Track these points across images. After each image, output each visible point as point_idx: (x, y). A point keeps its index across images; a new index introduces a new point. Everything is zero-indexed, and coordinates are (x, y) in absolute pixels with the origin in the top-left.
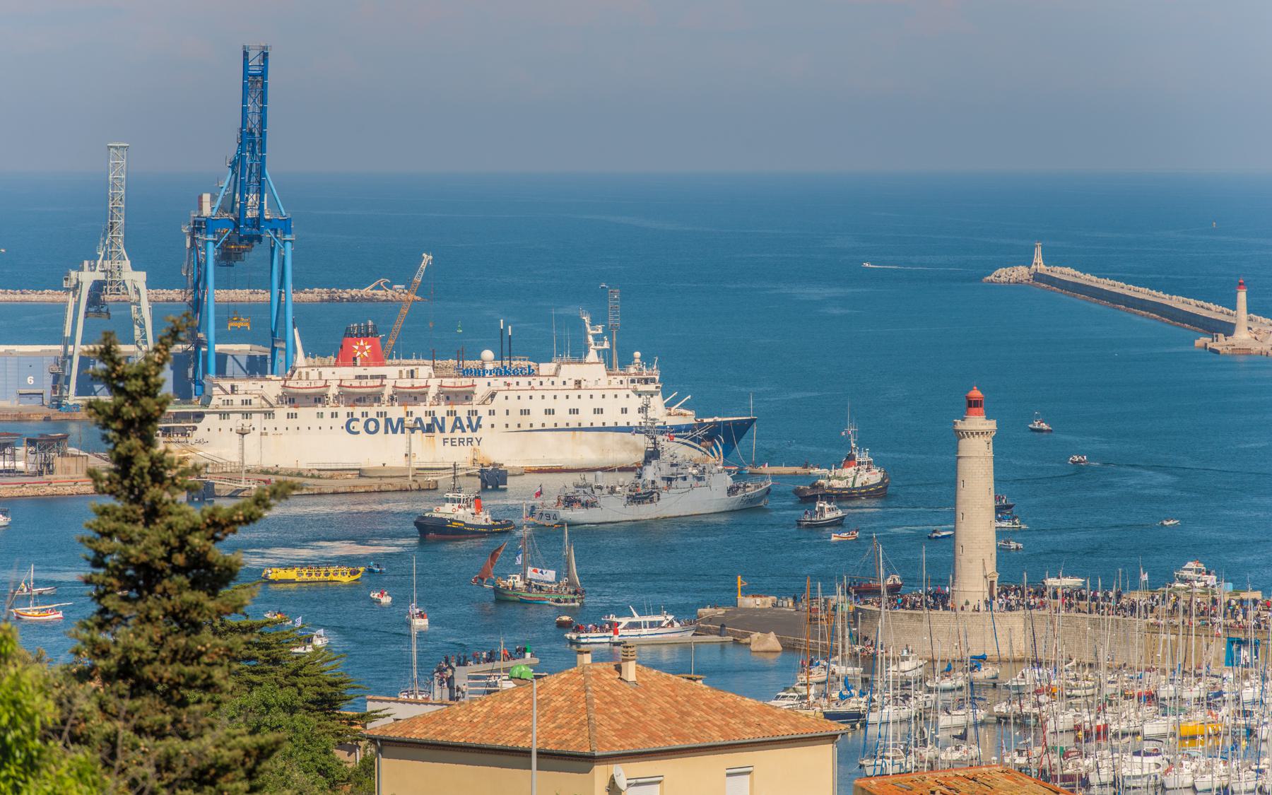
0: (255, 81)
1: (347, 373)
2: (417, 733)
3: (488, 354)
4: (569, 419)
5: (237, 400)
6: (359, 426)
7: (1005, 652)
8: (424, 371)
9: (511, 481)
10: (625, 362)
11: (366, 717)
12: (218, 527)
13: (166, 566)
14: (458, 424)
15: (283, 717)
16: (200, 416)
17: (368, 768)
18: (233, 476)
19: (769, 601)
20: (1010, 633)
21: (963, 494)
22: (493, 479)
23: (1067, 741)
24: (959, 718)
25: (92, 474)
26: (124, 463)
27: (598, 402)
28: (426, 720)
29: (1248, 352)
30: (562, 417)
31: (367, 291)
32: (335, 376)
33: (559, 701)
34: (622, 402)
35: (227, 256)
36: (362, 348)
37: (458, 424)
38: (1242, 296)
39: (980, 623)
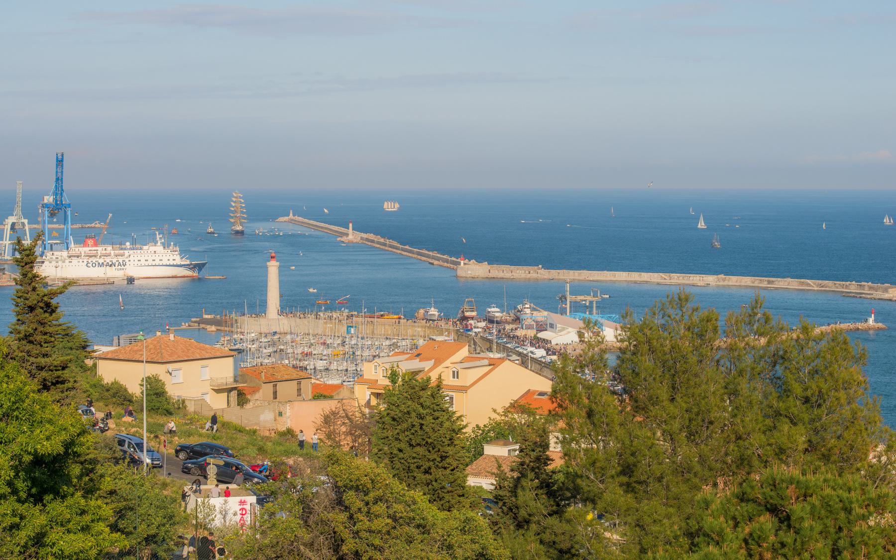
0: (60, 162)
1: (87, 249)
2: (109, 356)
3: (128, 244)
4: (154, 264)
5: (54, 257)
6: (90, 265)
7: (282, 330)
8: (109, 248)
9: (136, 282)
10: (169, 246)
11: (94, 351)
12: (53, 294)
13: (38, 304)
14: (119, 264)
15: (70, 351)
16: (43, 262)
17: (95, 365)
18: (54, 280)
19: (212, 316)
20: (285, 324)
21: (269, 275)
22: (131, 280)
23: (300, 357)
24: (270, 350)
25: (15, 279)
26: (25, 275)
27: (161, 258)
28: (112, 352)
29: (352, 242)
30: (150, 262)
31: (93, 225)
32: (84, 250)
33: (151, 346)
34: (168, 257)
35: (52, 215)
36: (90, 242)
37: (119, 264)
38: (351, 225)
39: (273, 318)
